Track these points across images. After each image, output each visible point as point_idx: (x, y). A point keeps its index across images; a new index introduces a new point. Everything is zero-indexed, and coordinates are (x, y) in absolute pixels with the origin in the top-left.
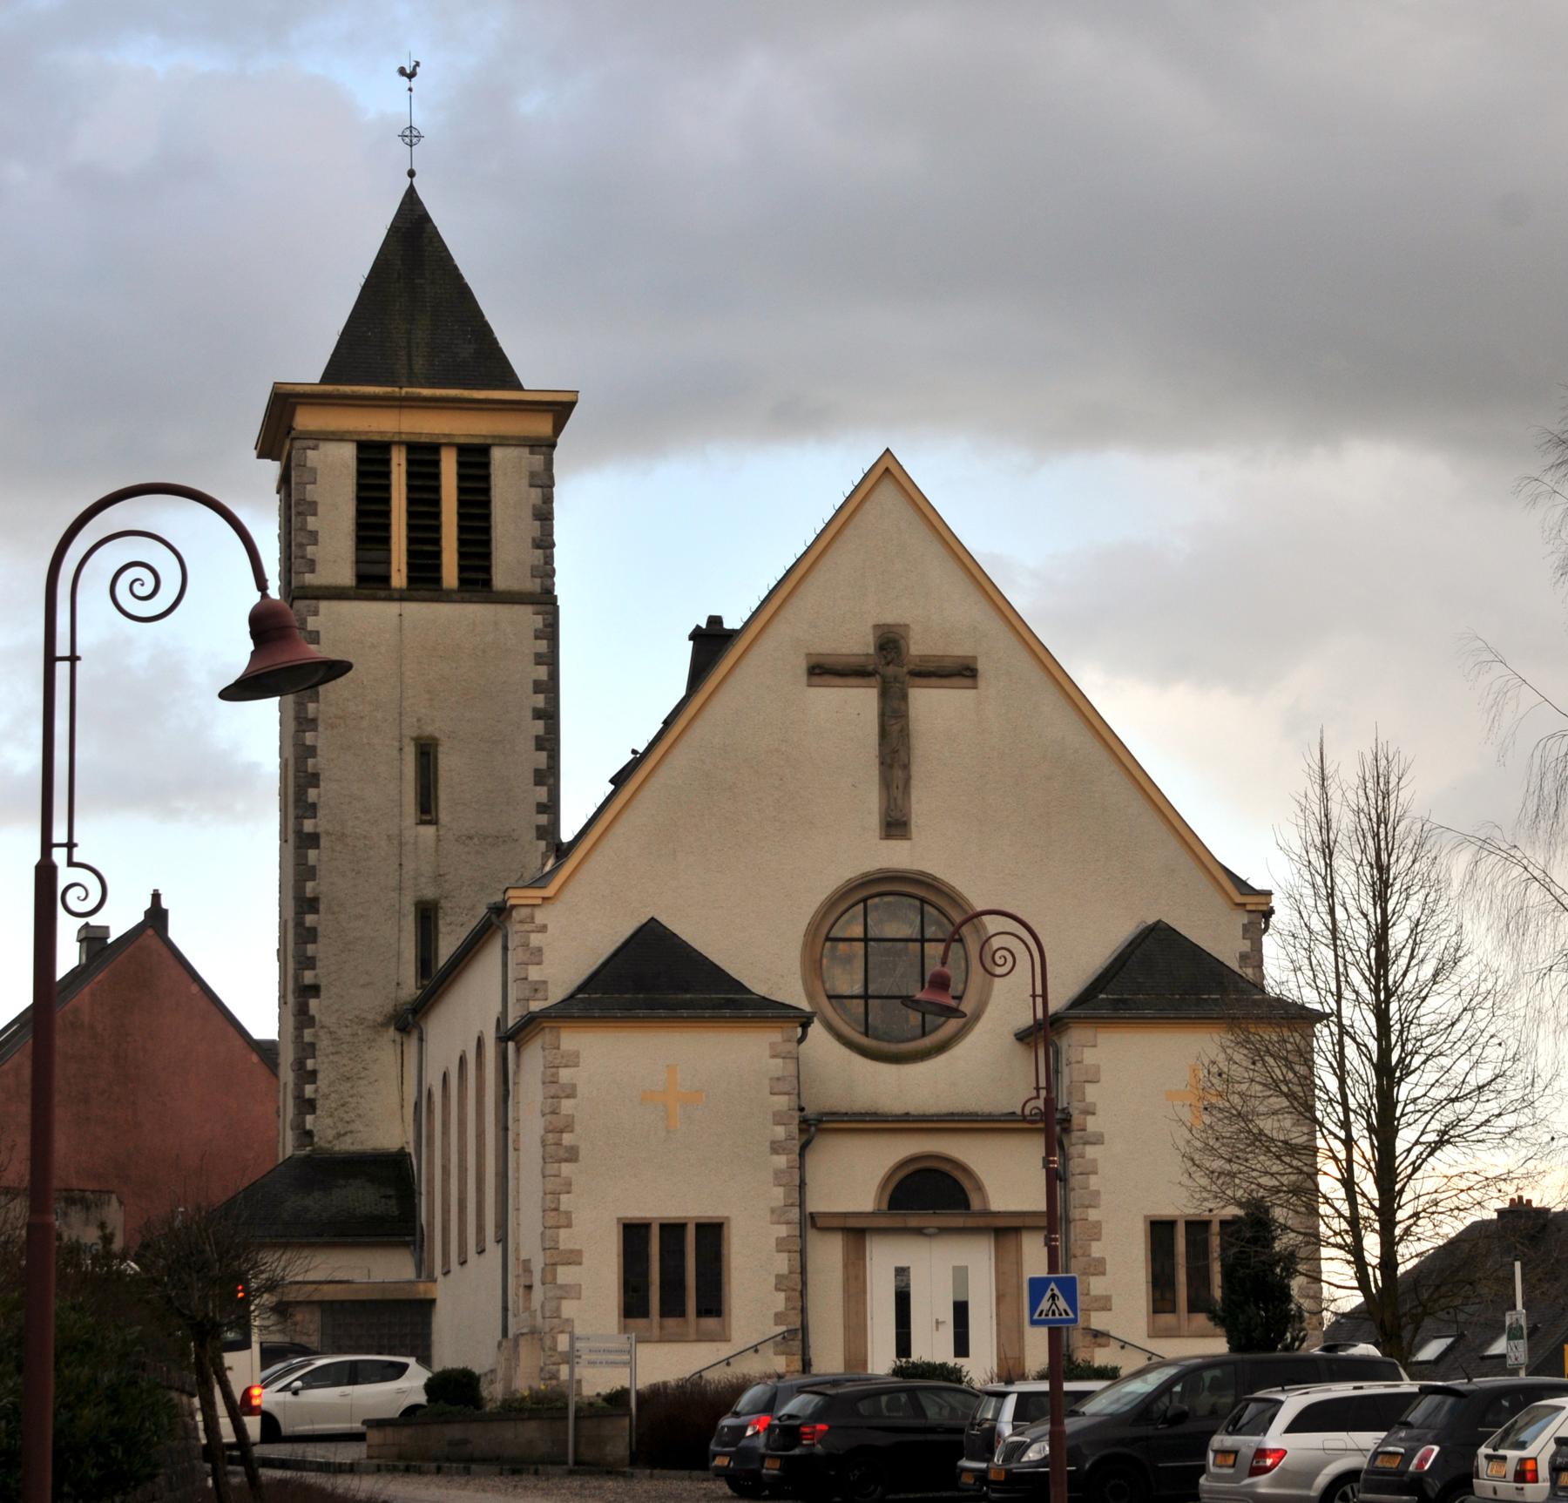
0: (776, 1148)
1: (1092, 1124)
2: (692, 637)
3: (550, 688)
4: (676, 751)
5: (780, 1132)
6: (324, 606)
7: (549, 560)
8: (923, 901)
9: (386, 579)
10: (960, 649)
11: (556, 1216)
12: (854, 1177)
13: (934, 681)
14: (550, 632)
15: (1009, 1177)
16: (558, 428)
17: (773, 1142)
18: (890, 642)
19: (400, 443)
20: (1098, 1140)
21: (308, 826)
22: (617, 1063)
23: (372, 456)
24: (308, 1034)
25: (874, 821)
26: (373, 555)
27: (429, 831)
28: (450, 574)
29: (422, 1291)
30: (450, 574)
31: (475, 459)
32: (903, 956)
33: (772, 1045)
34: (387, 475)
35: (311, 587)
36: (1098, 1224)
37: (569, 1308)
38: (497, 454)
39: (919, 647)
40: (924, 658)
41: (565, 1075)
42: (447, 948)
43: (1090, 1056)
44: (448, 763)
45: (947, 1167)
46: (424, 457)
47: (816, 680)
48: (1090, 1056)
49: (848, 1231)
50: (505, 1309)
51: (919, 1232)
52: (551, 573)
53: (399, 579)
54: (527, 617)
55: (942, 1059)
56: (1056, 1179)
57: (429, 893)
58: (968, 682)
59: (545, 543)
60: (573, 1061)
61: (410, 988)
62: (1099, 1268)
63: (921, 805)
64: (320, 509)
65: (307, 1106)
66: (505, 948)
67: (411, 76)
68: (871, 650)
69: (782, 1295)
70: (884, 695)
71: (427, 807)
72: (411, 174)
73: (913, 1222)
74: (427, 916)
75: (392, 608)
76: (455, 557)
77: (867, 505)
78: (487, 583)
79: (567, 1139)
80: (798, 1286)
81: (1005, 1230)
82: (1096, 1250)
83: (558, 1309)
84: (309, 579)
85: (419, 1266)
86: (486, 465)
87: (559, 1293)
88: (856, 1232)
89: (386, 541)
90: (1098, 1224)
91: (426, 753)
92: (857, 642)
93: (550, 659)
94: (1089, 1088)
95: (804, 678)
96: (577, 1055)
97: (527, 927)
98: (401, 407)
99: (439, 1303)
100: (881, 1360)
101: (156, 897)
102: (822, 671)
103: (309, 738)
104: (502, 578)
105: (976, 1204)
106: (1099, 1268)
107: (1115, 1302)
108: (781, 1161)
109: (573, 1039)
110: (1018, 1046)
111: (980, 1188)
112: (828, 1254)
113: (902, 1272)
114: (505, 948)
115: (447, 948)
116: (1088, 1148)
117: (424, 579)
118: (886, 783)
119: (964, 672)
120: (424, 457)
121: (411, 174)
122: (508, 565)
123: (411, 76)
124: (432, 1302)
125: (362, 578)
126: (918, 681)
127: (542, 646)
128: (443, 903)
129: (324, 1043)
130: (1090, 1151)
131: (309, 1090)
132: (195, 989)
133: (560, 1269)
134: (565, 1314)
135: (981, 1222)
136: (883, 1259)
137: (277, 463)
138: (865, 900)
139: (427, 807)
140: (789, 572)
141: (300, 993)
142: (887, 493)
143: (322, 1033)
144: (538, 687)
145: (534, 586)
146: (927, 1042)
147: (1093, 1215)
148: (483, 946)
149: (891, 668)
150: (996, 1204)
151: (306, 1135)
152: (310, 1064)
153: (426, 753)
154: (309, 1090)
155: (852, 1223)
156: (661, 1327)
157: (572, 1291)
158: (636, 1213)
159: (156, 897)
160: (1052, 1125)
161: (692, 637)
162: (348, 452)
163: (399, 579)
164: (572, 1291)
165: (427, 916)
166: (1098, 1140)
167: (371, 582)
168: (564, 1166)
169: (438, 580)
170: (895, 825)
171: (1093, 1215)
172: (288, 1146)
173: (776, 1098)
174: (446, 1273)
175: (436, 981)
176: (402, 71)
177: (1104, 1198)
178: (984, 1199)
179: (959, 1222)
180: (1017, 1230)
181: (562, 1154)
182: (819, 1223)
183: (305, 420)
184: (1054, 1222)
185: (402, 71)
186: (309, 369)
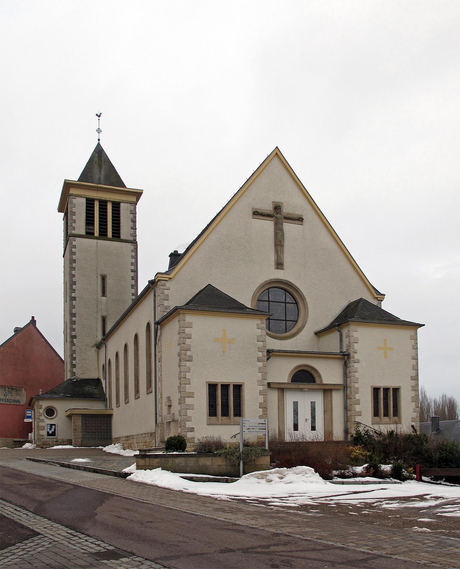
0: (259, 360)
1: (356, 356)
2: (170, 256)
3: (136, 264)
4: (212, 234)
5: (260, 354)
6: (77, 239)
7: (135, 232)
8: (286, 291)
9: (93, 234)
10: (298, 212)
11: (183, 380)
12: (283, 371)
13: (290, 221)
14: (136, 250)
15: (330, 373)
16: (138, 199)
17: (258, 358)
18: (277, 208)
19: (97, 199)
20: (358, 362)
21: (73, 295)
22: (204, 328)
23: (90, 203)
24: (74, 348)
25: (273, 263)
26: (90, 227)
27: (104, 299)
28: (110, 234)
29: (108, 412)
30: (110, 234)
31: (116, 206)
32: (279, 305)
33: (258, 325)
34: (94, 207)
35: (74, 234)
36: (358, 389)
37: (190, 413)
38: (122, 205)
39: (286, 210)
40: (291, 211)
41: (187, 330)
42: (108, 328)
43: (355, 335)
44: (109, 281)
45: (309, 369)
46: (103, 204)
47: (255, 216)
48: (355, 335)
49: (279, 389)
50: (156, 414)
51: (301, 390)
52: (136, 236)
53: (97, 234)
54: (130, 246)
55: (298, 337)
56: (346, 375)
57: (104, 314)
58: (300, 223)
59: (134, 228)
60: (190, 326)
61: (100, 337)
62: (358, 402)
63: (287, 260)
64: (76, 214)
65: (74, 366)
66: (155, 296)
67: (99, 116)
68: (272, 209)
69: (261, 409)
70: (276, 224)
71: (104, 294)
72: (99, 140)
73: (301, 386)
74: (104, 320)
75: (95, 241)
76: (111, 230)
77: (270, 164)
78: (119, 237)
79: (188, 353)
80: (264, 407)
81: (327, 391)
82: (357, 396)
83: (186, 413)
84: (73, 232)
85: (106, 406)
86: (119, 207)
87: (187, 407)
88: (281, 389)
89: (93, 224)
90: (358, 389)
91: (104, 278)
92: (268, 208)
93: (136, 257)
94: (355, 345)
95: (251, 215)
96: (191, 323)
97: (163, 287)
98: (97, 190)
99: (114, 415)
100: (338, 434)
101: (33, 317)
102: (257, 214)
103: (73, 272)
104: (123, 237)
105: (318, 381)
106: (358, 402)
107: (363, 413)
108: (261, 364)
109: (189, 318)
110: (315, 336)
111: (320, 376)
112: (274, 396)
113: (296, 404)
114: (155, 296)
115: (108, 328)
116: (355, 364)
117: (103, 234)
118: (277, 251)
119: (300, 220)
120: (103, 204)
121: (99, 140)
122: (125, 233)
123: (99, 116)
124: (110, 416)
125: (87, 233)
126: (286, 221)
127: (133, 254)
128: (108, 317)
129: (78, 350)
130: (356, 365)
131: (74, 362)
132: (43, 340)
133: (186, 399)
134: (188, 415)
135: (319, 387)
136: (290, 399)
137: (63, 214)
138: (268, 289)
139: (104, 294)
140: (218, 215)
141: (71, 338)
142: (276, 161)
143: (77, 348)
144: (132, 264)
145: (131, 239)
146: (288, 334)
147: (357, 385)
148: (145, 298)
149: (277, 215)
150: (325, 382)
151: (73, 374)
152: (74, 355)
153: (104, 278)
154: (74, 362)
155: (282, 386)
156: (222, 420)
157: (191, 407)
158: (213, 380)
159: (33, 317)
160: (345, 358)
161: (170, 256)
162: (84, 201)
163: (97, 234)
164: (191, 407)
165: (104, 320)
166: (358, 362)
167: (89, 234)
168: (187, 362)
169: (106, 235)
170: (279, 265)
171: (357, 385)
172: (68, 376)
173: (259, 343)
174: (118, 407)
175: (106, 336)
176: (97, 115)
177: (360, 380)
178: (321, 380)
179: (315, 387)
180: (331, 390)
181: (187, 358)
182: (272, 386)
183: (72, 191)
184: (344, 387)
185: (97, 115)
186: (75, 177)
